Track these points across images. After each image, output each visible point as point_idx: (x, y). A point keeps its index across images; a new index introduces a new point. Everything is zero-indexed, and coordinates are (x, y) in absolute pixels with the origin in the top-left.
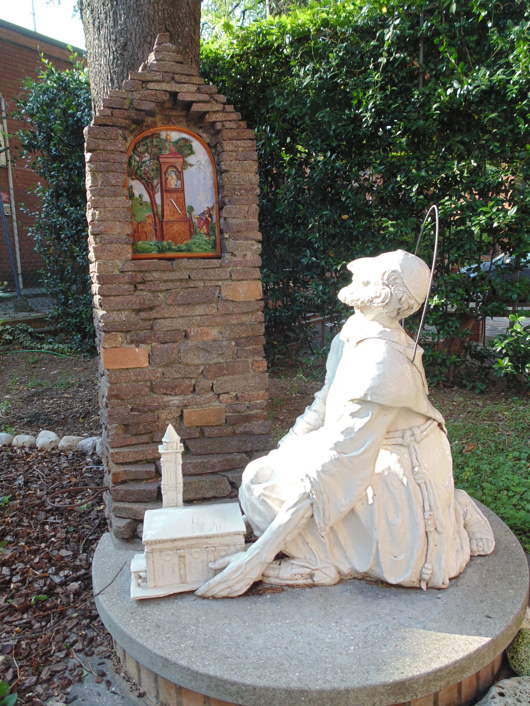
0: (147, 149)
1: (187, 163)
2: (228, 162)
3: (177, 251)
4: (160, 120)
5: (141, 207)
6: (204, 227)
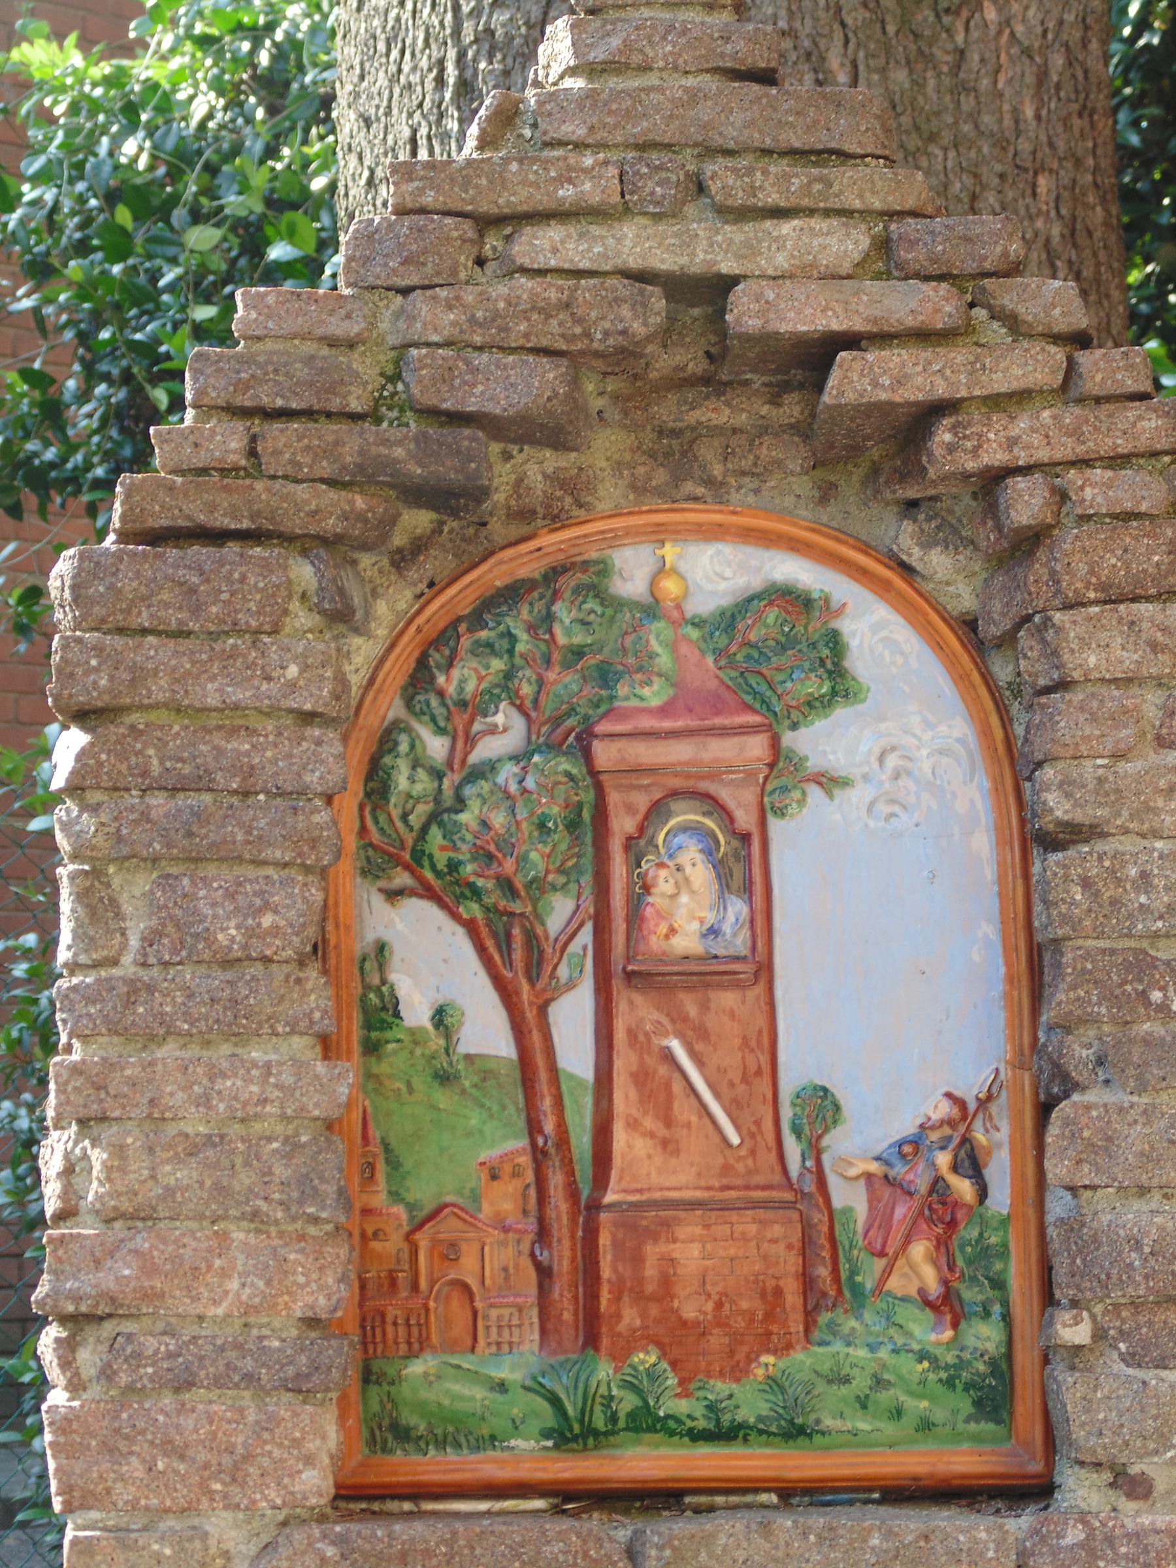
0: (508, 675)
1: (797, 763)
2: (1089, 770)
3: (697, 1436)
4: (618, 466)
5: (443, 1098)
6: (919, 1250)
